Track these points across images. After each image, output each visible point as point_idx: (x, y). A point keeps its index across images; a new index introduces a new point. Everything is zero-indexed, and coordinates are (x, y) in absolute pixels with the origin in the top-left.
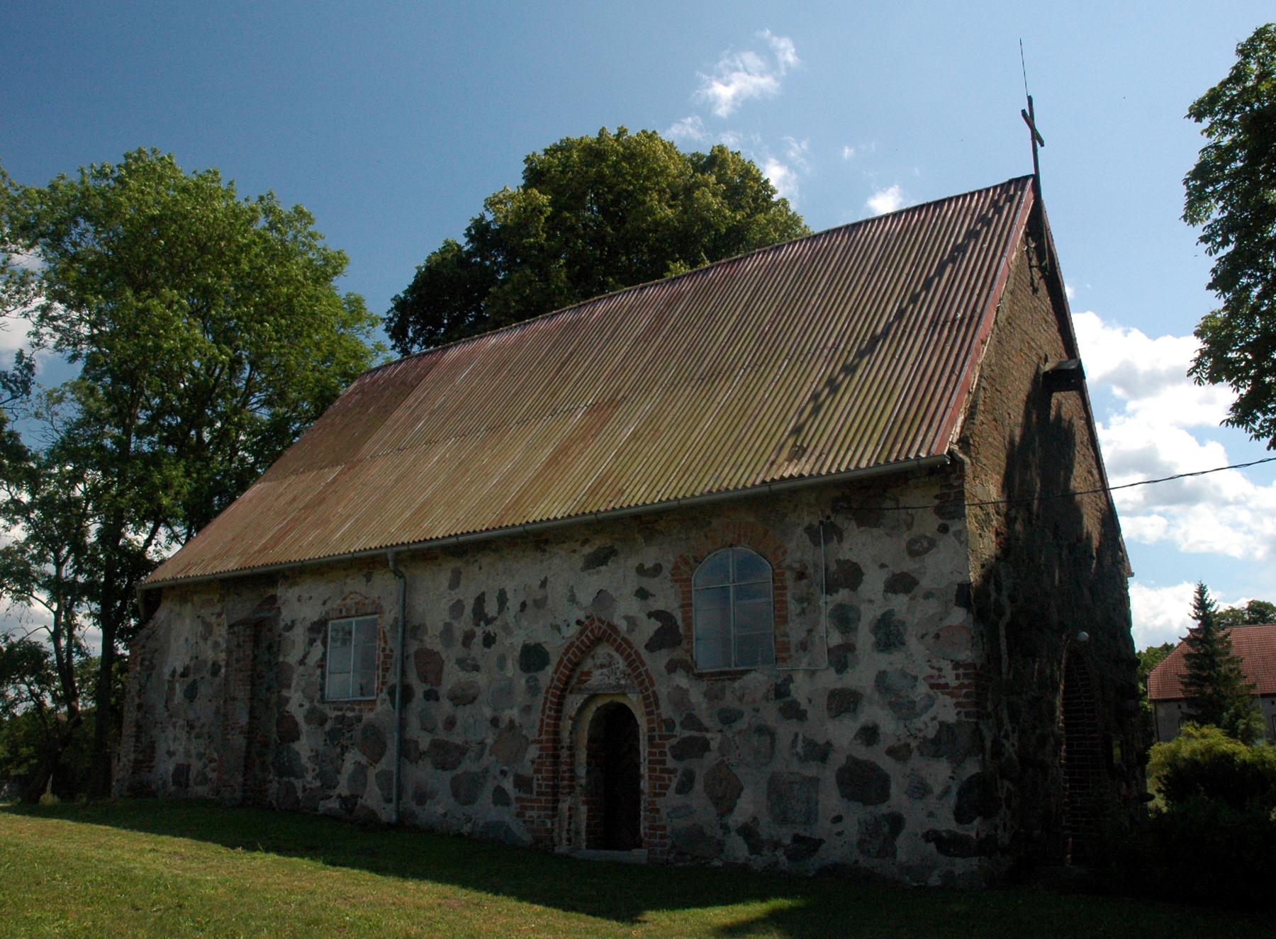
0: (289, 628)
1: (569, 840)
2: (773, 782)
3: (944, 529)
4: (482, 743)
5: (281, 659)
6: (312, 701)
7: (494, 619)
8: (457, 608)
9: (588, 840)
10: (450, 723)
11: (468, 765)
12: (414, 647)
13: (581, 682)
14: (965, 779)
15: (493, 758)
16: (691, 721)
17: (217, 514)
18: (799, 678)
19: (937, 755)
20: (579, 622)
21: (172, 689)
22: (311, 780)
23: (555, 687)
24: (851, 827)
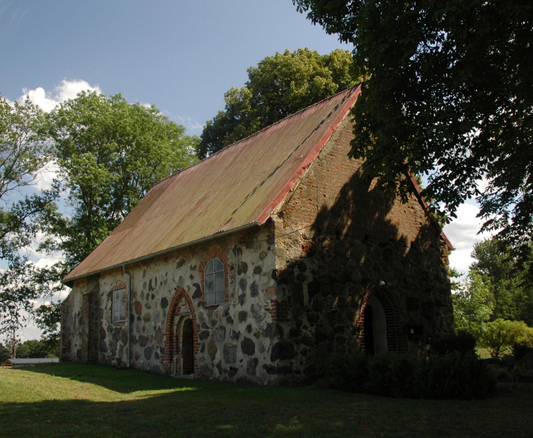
0: (102, 295)
1: (177, 371)
2: (225, 346)
3: (269, 249)
4: (152, 336)
5: (100, 307)
6: (109, 323)
7: (154, 288)
8: (145, 284)
9: (184, 371)
10: (144, 329)
11: (149, 345)
12: (134, 300)
13: (179, 311)
14: (274, 345)
15: (155, 341)
16: (204, 325)
17: (92, 250)
18: (231, 307)
19: (266, 336)
20: (175, 289)
21: (75, 320)
22: (109, 353)
23: (170, 314)
24: (245, 363)
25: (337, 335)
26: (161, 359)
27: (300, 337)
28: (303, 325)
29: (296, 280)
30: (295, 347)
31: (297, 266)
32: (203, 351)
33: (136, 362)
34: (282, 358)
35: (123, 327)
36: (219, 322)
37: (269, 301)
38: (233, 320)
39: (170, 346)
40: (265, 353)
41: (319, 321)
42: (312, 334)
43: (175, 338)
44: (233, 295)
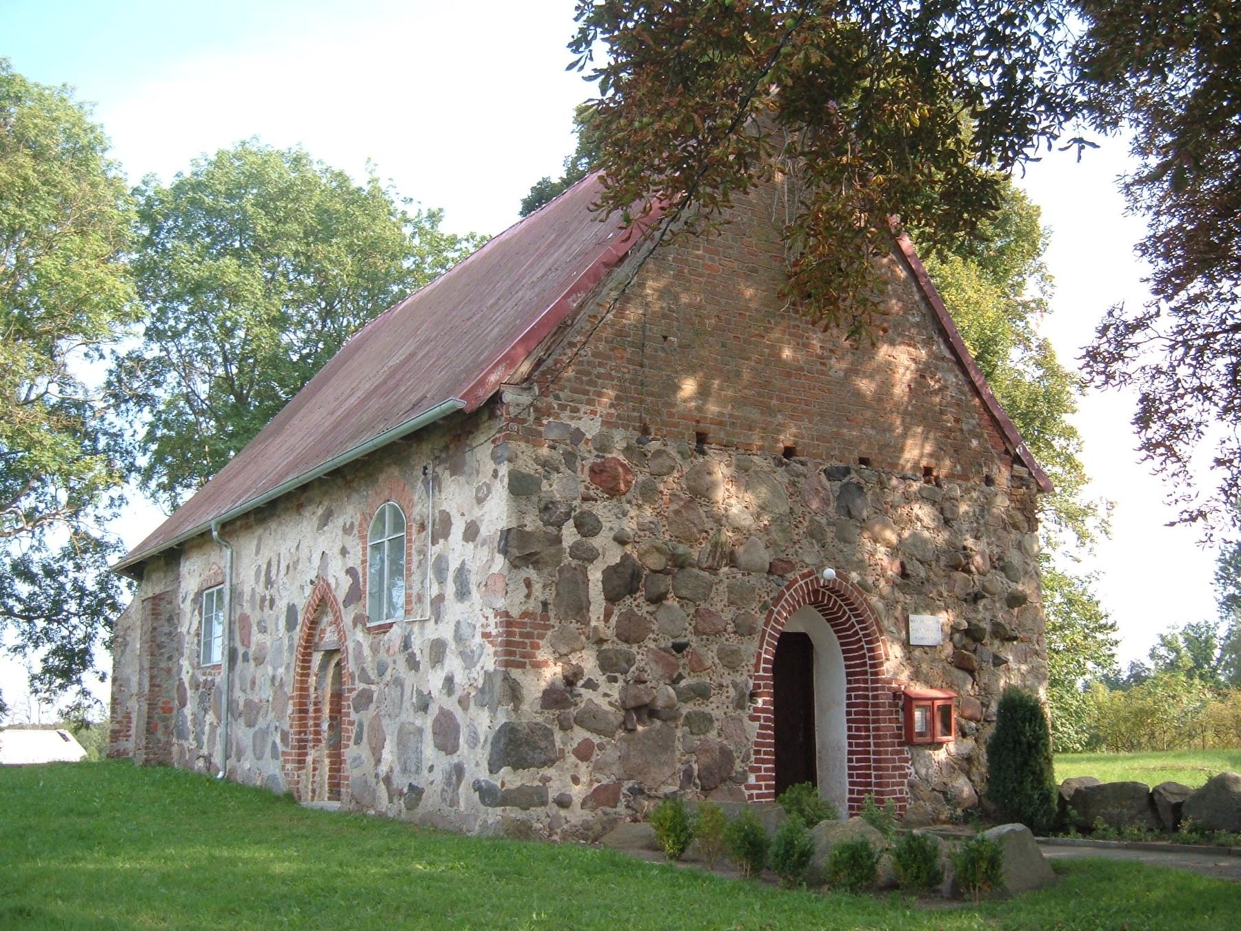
24: (438, 776)
25: (686, 709)
26: (282, 759)
27: (573, 711)
28: (585, 679)
29: (567, 560)
30: (558, 736)
31: (571, 522)
32: (358, 741)
33: (238, 765)
34: (519, 764)
35: (218, 680)
36: (391, 666)
37: (490, 613)
38: (419, 663)
39: (300, 726)
40: (478, 749)
41: (633, 669)
42: (610, 704)
43: (311, 708)
44: (420, 599)
